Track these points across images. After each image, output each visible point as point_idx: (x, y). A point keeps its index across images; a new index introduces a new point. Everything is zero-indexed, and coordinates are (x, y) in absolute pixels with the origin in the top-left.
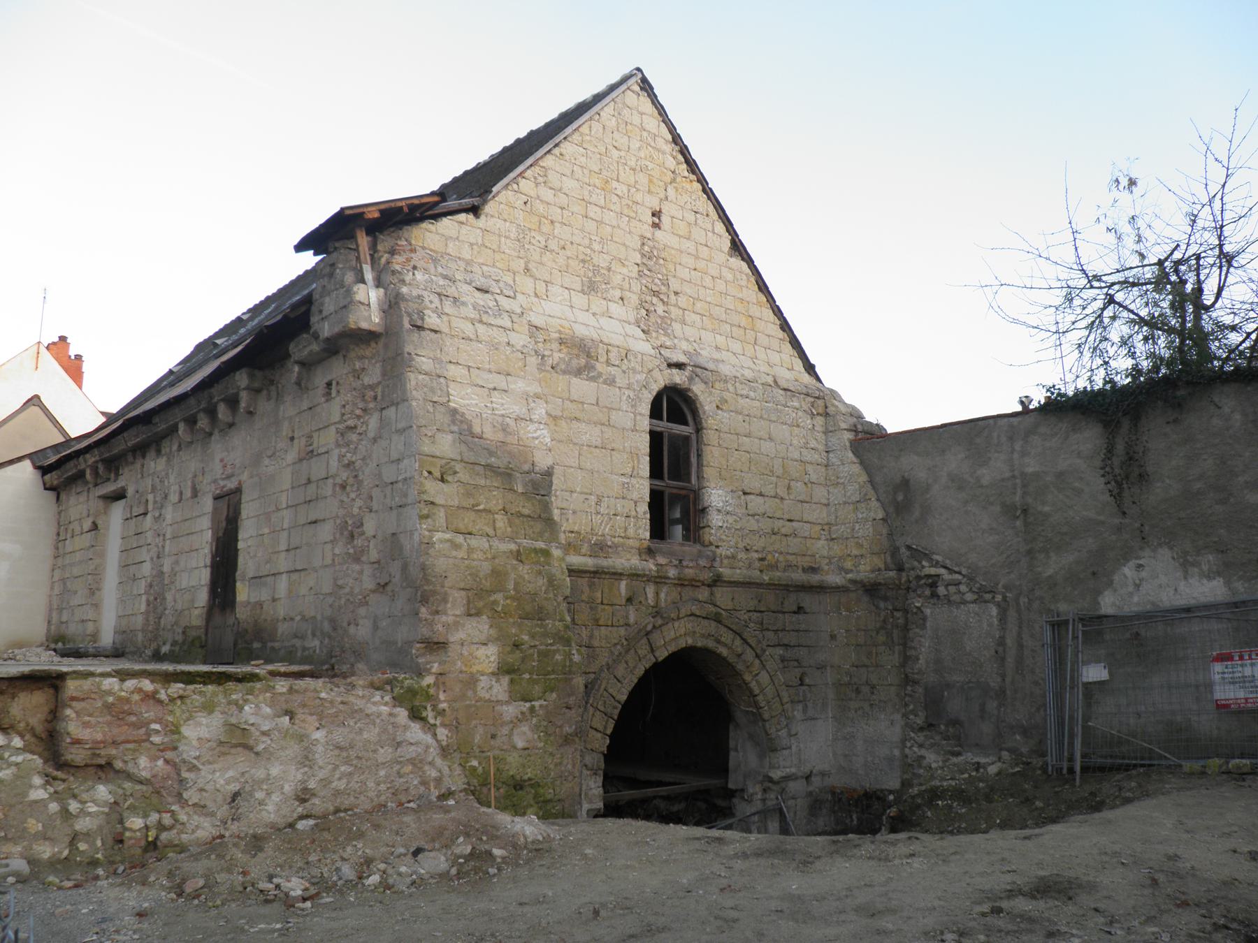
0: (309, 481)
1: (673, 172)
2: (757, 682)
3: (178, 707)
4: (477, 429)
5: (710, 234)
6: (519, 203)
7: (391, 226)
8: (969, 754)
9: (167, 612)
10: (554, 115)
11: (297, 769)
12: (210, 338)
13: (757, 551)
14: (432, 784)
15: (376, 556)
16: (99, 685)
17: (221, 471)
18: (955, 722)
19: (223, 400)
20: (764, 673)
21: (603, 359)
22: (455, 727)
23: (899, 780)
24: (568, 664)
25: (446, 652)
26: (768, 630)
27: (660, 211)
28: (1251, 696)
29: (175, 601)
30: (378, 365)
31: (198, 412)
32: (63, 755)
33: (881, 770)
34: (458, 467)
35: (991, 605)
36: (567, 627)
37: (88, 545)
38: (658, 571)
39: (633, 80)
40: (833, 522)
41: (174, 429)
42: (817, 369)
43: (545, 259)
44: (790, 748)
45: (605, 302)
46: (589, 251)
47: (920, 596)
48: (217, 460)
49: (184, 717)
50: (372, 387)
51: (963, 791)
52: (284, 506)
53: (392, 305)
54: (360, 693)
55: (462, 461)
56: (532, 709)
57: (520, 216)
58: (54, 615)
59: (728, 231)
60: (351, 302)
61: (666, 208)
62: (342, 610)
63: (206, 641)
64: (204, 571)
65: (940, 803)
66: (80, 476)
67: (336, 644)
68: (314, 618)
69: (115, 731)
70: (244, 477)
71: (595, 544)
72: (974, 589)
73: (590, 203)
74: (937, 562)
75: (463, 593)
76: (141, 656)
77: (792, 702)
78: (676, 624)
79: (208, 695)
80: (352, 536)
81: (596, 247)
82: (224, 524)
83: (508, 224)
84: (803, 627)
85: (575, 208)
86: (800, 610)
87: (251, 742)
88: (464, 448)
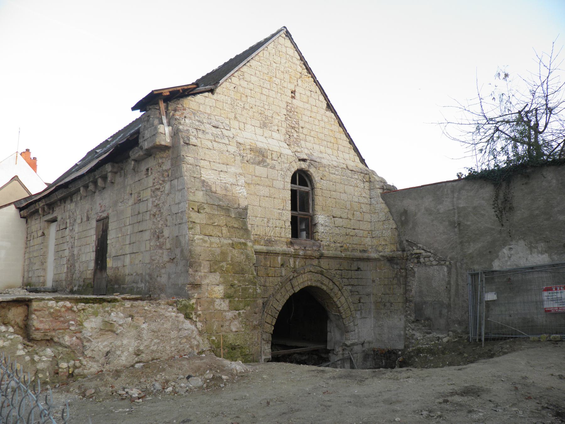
0: (139, 213)
2: (340, 301)
3: (82, 314)
4: (214, 189)
5: (317, 101)
6: (232, 88)
7: (174, 99)
9: (76, 272)
10: (247, 48)
11: (135, 341)
12: (94, 149)
16: (47, 304)
17: (100, 209)
18: (428, 319)
19: (100, 177)
21: (270, 157)
22: (205, 322)
25: (201, 289)
27: (295, 91)
28: (560, 306)
30: (169, 161)
31: (89, 182)
32: (31, 335)
34: (205, 206)
35: (444, 266)
36: (254, 277)
38: (295, 252)
41: (79, 190)
42: (366, 161)
43: (243, 113)
44: (355, 331)
46: (263, 109)
47: (412, 263)
48: (98, 204)
50: (167, 171)
51: (432, 350)
53: (175, 134)
54: (163, 307)
55: (207, 203)
56: (239, 314)
57: (232, 93)
58: (26, 274)
59: (325, 99)
60: (157, 133)
62: (154, 270)
64: (92, 253)
65: (422, 355)
66: (37, 211)
67: (152, 285)
68: (142, 274)
69: (54, 324)
70: (110, 211)
71: (267, 240)
74: (420, 247)
78: (303, 276)
79: (95, 308)
80: (158, 237)
81: (266, 107)
82: (101, 233)
84: (360, 277)
86: (358, 269)
87: (115, 329)
88: (208, 197)
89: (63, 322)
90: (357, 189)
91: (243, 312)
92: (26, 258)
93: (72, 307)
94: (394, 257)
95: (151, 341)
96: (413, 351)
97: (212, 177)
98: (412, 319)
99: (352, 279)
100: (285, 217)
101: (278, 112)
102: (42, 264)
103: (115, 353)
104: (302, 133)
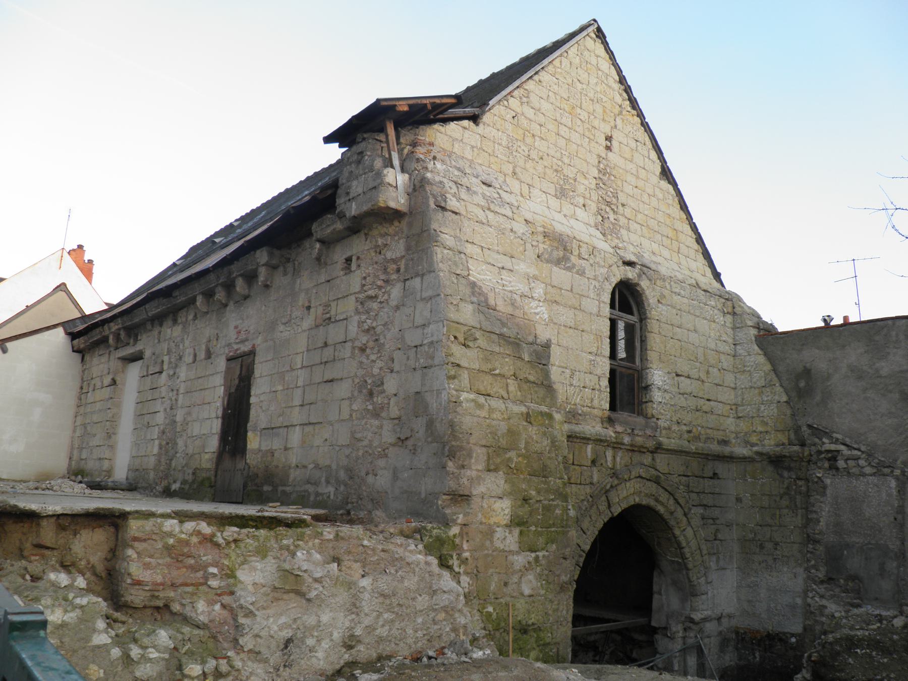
0: (326, 345)
1: (620, 106)
2: (685, 536)
3: (232, 551)
4: (492, 302)
5: (647, 160)
6: (509, 117)
7: (410, 125)
8: (869, 607)
9: (178, 455)
10: (515, 59)
11: (346, 616)
12: (212, 236)
13: (685, 425)
14: (461, 631)
15: (397, 412)
16: (161, 526)
17: (235, 337)
18: (854, 578)
19: (241, 275)
20: (689, 529)
21: (576, 253)
22: (475, 575)
23: (802, 625)
24: (565, 518)
25: (469, 504)
26: (692, 492)
27: (611, 137)
29: (186, 446)
30: (401, 241)
31: (216, 286)
32: (123, 596)
33: (783, 616)
34: (478, 334)
35: (889, 478)
36: (565, 484)
37: (107, 397)
38: (616, 438)
39: (591, 29)
40: (739, 403)
41: (193, 301)
42: (722, 277)
44: (707, 593)
45: (572, 207)
47: (820, 468)
48: (232, 328)
49: (240, 560)
50: (394, 261)
51: (879, 642)
52: (299, 366)
53: (418, 187)
54: (399, 542)
55: (480, 328)
56: (537, 559)
57: (510, 127)
58: (76, 453)
59: (659, 158)
60: (382, 183)
61: (616, 135)
62: (360, 461)
63: (215, 482)
64: (215, 421)
65: (859, 651)
66: (104, 341)
67: (353, 491)
68: (329, 466)
69: (175, 573)
70: (259, 341)
71: (569, 412)
72: (873, 464)
73: (561, 124)
74: (837, 440)
75: (484, 450)
76: (152, 491)
77: (709, 554)
78: (628, 484)
79: (262, 539)
80: (371, 394)
81: (566, 161)
82: (237, 382)
83: (500, 133)
84: (717, 490)
85: (551, 127)
86: (715, 476)
87: (304, 589)
88: (482, 317)
89: (193, 569)
90: (713, 325)
91: (544, 556)
92: (78, 423)
93: (213, 535)
94: (785, 456)
95: (378, 617)
96: (837, 641)
97: (488, 278)
98: (820, 575)
99: (704, 495)
100: (599, 369)
101: (585, 171)
102: (109, 436)
103: (303, 642)
104: (623, 215)
